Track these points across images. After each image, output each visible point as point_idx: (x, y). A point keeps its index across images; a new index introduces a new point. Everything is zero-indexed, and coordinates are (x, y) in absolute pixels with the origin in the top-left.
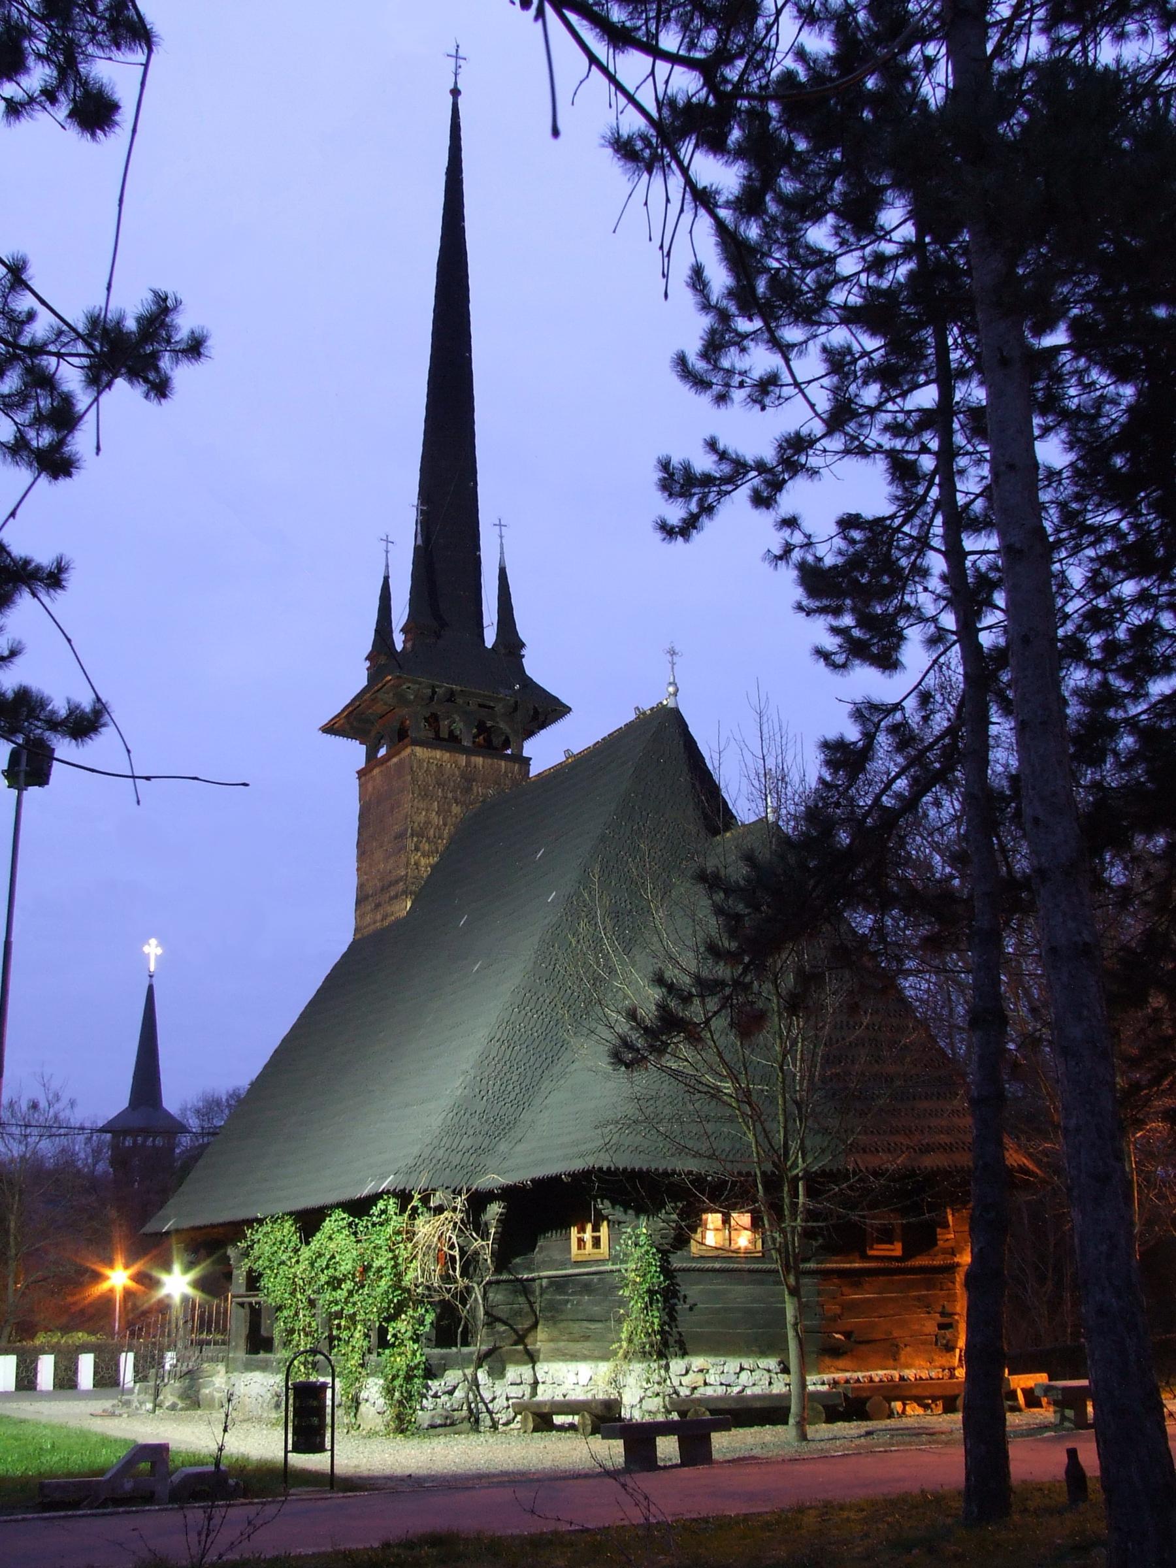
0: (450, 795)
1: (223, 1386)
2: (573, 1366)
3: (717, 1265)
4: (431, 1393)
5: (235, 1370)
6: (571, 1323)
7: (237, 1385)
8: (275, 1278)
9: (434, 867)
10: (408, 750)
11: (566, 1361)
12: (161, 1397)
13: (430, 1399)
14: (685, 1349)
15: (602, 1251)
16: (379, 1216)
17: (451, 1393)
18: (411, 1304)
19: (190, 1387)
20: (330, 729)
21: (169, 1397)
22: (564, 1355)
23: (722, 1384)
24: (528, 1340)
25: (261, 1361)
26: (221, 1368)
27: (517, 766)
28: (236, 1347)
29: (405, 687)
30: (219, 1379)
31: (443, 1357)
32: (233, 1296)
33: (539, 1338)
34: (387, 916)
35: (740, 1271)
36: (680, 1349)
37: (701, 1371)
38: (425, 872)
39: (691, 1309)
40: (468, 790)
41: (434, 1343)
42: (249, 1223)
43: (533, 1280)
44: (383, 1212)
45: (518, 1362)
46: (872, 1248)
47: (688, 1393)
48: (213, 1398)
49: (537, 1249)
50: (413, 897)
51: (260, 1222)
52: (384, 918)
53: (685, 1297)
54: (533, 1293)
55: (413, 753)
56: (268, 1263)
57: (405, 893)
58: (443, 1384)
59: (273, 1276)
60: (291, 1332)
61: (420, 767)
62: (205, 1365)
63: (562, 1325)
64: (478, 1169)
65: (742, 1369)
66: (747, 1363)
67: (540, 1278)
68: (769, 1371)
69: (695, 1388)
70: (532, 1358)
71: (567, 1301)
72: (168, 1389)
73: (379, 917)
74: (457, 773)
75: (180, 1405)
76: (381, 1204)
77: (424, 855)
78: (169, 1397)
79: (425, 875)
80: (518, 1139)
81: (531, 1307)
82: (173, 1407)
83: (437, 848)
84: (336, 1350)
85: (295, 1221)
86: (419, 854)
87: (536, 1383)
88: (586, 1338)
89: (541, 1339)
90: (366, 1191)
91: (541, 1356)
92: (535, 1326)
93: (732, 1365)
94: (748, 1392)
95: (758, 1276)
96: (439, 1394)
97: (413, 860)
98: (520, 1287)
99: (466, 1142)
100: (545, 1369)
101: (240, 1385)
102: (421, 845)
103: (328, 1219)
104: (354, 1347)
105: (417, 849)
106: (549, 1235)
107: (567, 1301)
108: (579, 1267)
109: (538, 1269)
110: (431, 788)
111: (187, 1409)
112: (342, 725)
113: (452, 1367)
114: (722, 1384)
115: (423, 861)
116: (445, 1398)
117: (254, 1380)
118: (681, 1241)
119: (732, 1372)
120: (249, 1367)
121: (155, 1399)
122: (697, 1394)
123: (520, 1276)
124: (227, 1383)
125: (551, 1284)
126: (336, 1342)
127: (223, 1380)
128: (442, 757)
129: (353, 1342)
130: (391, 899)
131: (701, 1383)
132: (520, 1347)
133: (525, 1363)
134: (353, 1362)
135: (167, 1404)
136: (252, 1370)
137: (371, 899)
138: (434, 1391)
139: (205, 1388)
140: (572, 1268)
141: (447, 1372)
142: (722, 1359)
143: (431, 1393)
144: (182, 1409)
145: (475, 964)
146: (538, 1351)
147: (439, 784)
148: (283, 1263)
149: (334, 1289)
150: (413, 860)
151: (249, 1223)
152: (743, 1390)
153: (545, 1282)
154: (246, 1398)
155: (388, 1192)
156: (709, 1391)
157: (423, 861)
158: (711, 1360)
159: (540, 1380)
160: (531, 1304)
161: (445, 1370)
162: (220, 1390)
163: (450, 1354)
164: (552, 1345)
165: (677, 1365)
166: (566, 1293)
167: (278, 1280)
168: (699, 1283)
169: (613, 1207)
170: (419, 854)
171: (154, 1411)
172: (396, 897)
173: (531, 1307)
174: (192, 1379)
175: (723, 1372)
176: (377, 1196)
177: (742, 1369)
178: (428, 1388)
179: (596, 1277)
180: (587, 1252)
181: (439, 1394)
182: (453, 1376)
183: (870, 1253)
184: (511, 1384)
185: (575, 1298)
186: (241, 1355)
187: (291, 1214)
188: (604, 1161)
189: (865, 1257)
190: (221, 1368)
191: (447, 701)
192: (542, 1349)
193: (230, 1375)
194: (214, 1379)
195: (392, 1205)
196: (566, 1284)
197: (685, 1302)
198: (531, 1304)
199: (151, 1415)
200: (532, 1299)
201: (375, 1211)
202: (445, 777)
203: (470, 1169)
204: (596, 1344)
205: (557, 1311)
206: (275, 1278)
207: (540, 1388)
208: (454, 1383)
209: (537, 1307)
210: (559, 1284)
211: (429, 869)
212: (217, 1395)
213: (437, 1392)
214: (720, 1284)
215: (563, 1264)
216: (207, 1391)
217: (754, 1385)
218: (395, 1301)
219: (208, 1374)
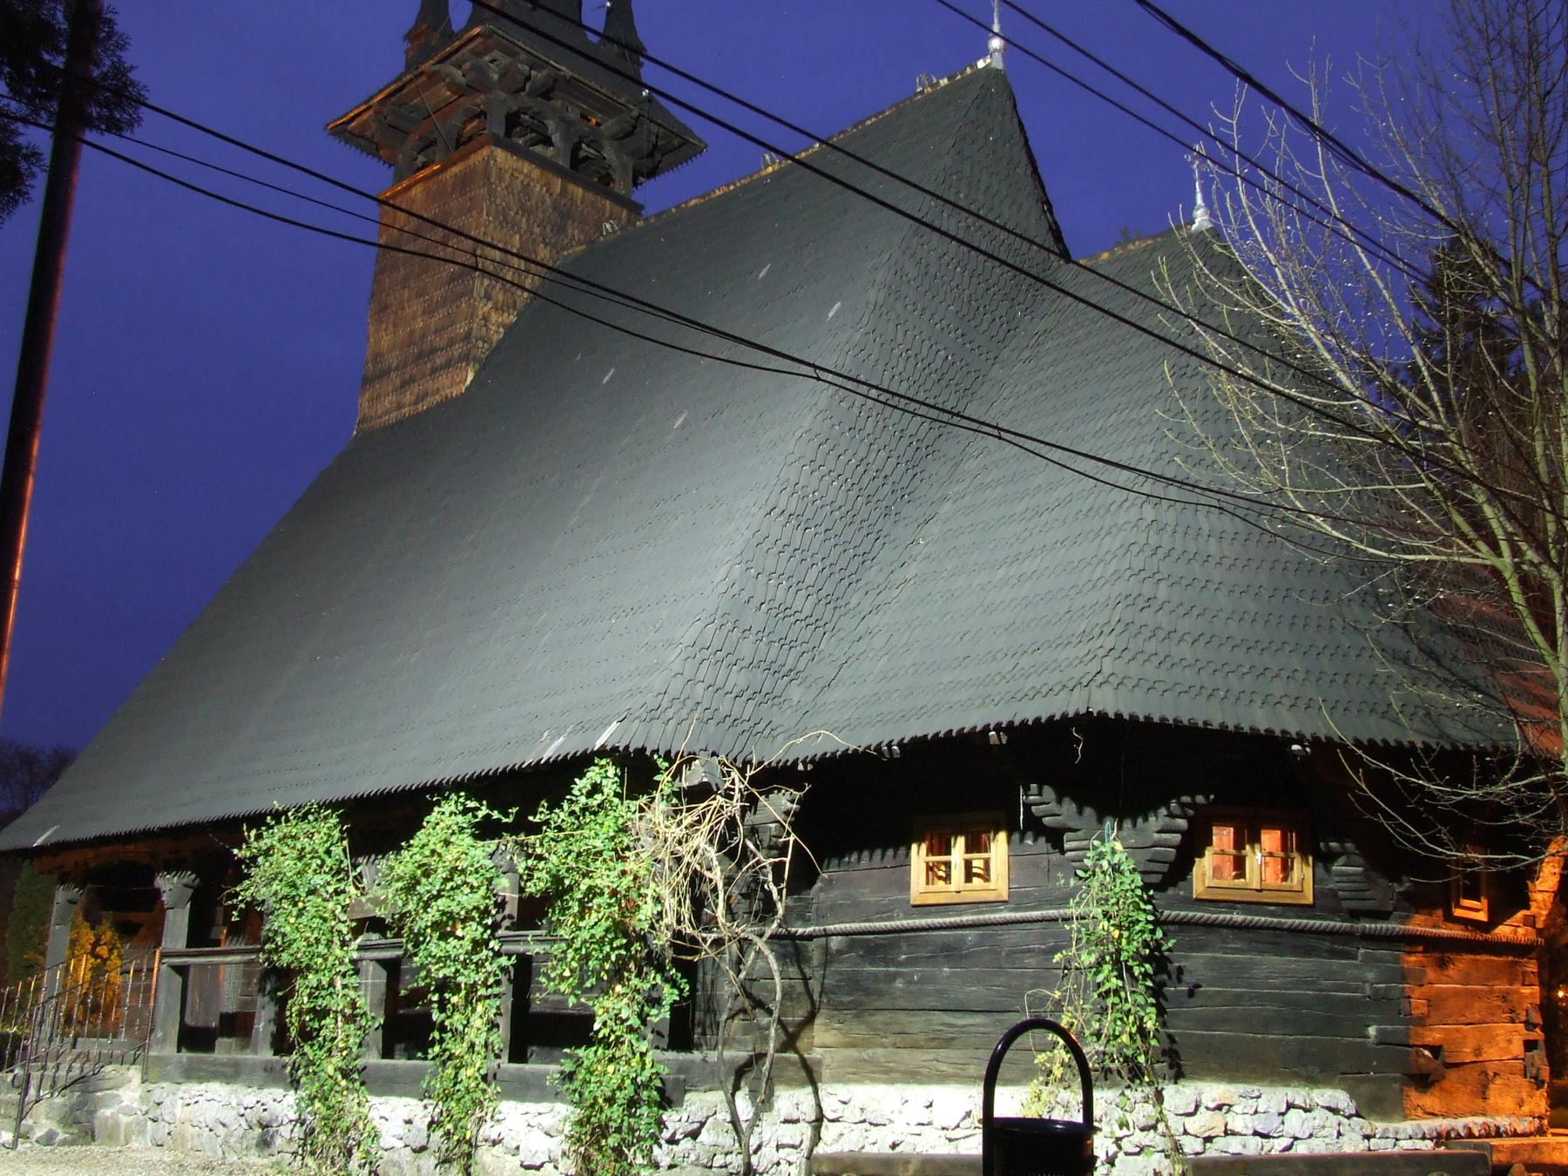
0: (537, 230)
1: (135, 1105)
2: (918, 1093)
3: (1238, 917)
4: (666, 1134)
5: (164, 1077)
6: (902, 1016)
7: (167, 1102)
8: (298, 917)
9: (510, 329)
10: (485, 152)
11: (893, 1082)
12: (28, 1121)
13: (665, 1146)
14: (1179, 1066)
15: (991, 885)
16: (590, 795)
17: (694, 1135)
18: (632, 965)
19: (81, 1105)
20: (341, 131)
21: (42, 1121)
22: (888, 1071)
23: (1256, 1133)
24: (801, 1044)
25: (224, 1064)
26: (134, 1073)
27: (624, 214)
28: (164, 1040)
29: (487, 58)
30: (129, 1093)
31: (682, 1068)
32: (163, 955)
33: (817, 1040)
34: (427, 395)
35: (1268, 928)
36: (1171, 1066)
37: (1219, 1108)
38: (497, 334)
39: (1191, 993)
40: (561, 229)
41: (667, 1039)
42: (257, 821)
43: (810, 937)
44: (596, 789)
45: (792, 1083)
46: (1459, 906)
47: (1199, 1148)
48: (117, 1124)
49: (819, 884)
50: (477, 366)
51: (278, 816)
52: (420, 398)
53: (1180, 970)
54: (808, 960)
55: (491, 156)
56: (286, 890)
57: (465, 358)
58: (685, 1118)
59: (295, 913)
60: (321, 1014)
61: (501, 179)
62: (109, 1068)
63: (880, 1018)
64: (760, 727)
65: (1290, 1106)
66: (1298, 1094)
67: (827, 935)
68: (1335, 1111)
69: (1208, 1139)
70: (810, 1075)
71: (894, 976)
72: (42, 1107)
73: (408, 397)
74: (548, 201)
75: (61, 1136)
76: (593, 774)
77: (496, 308)
78: (42, 1121)
79: (495, 338)
80: (822, 683)
81: (806, 985)
82: (49, 1139)
83: (515, 302)
84: (437, 1049)
85: (343, 819)
86: (490, 305)
87: (820, 1119)
88: (947, 1043)
89: (822, 1040)
90: (551, 749)
91: (826, 1073)
92: (810, 1019)
93: (1273, 1097)
94: (1301, 1149)
95: (1302, 940)
96: (678, 1136)
97: (480, 313)
98: (790, 949)
99: (738, 679)
100: (833, 1095)
101: (173, 1105)
102: (493, 293)
103: (436, 809)
104: (472, 1045)
105: (488, 297)
106: (854, 857)
107: (894, 976)
108: (927, 915)
109: (821, 918)
110: (512, 213)
111: (72, 1143)
112: (365, 124)
113: (694, 1087)
114: (1256, 1133)
115: (494, 317)
116: (686, 1144)
117: (209, 1096)
118: (1180, 868)
119: (1273, 1111)
120: (192, 1074)
121: (18, 1125)
122: (1212, 1152)
123: (793, 930)
124: (142, 1100)
125: (851, 946)
126: (436, 1035)
127: (137, 1095)
128: (530, 172)
129: (471, 1035)
130: (434, 371)
131: (1220, 1130)
132: (793, 1056)
133: (802, 1085)
134: (470, 1071)
135: (39, 1133)
136: (201, 1080)
137: (393, 375)
138: (671, 1131)
139: (105, 1106)
140: (906, 918)
141: (688, 1096)
142: (1254, 1089)
143: (666, 1134)
144: (64, 1143)
145: (677, 417)
146: (819, 1062)
147: (524, 209)
148: (312, 892)
149: (444, 937)
150: (480, 313)
151: (257, 821)
152: (1289, 1147)
153: (835, 942)
154: (188, 1124)
155: (602, 752)
156: (1234, 1146)
157: (494, 317)
158: (1241, 1088)
159: (828, 1114)
160: (805, 979)
161: (686, 1091)
162: (129, 1111)
163: (693, 1061)
164: (853, 1053)
165: (1178, 1095)
166: (887, 962)
167: (304, 920)
168: (1201, 948)
169: (1059, 801)
170: (490, 305)
171: (14, 1145)
172: (448, 365)
173: (806, 985)
174: (85, 1091)
175: (1256, 1112)
176: (578, 764)
177: (1290, 1106)
178: (661, 1124)
179: (971, 935)
180: (953, 887)
181: (678, 1136)
182: (700, 1103)
183: (1458, 912)
184: (786, 1121)
185: (916, 972)
186: (165, 1047)
187: (333, 805)
188: (1107, 702)
189: (1450, 918)
190: (134, 1073)
191: (540, 96)
192: (828, 1060)
193: (151, 1087)
194: (121, 1091)
195: (605, 775)
196: (892, 945)
197: (1180, 981)
198: (805, 979)
199: (12, 1153)
200: (808, 971)
201: (582, 785)
202: (533, 202)
203: (746, 726)
204: (969, 1053)
205: (868, 992)
206: (298, 917)
207: (828, 1131)
208: (700, 1117)
209: (815, 985)
210: (875, 947)
211: (501, 330)
212: (124, 1119)
213: (674, 1134)
214: (1236, 951)
215: (885, 912)
216: (108, 1112)
217: (1311, 1136)
218: (613, 958)
219: (112, 1083)
